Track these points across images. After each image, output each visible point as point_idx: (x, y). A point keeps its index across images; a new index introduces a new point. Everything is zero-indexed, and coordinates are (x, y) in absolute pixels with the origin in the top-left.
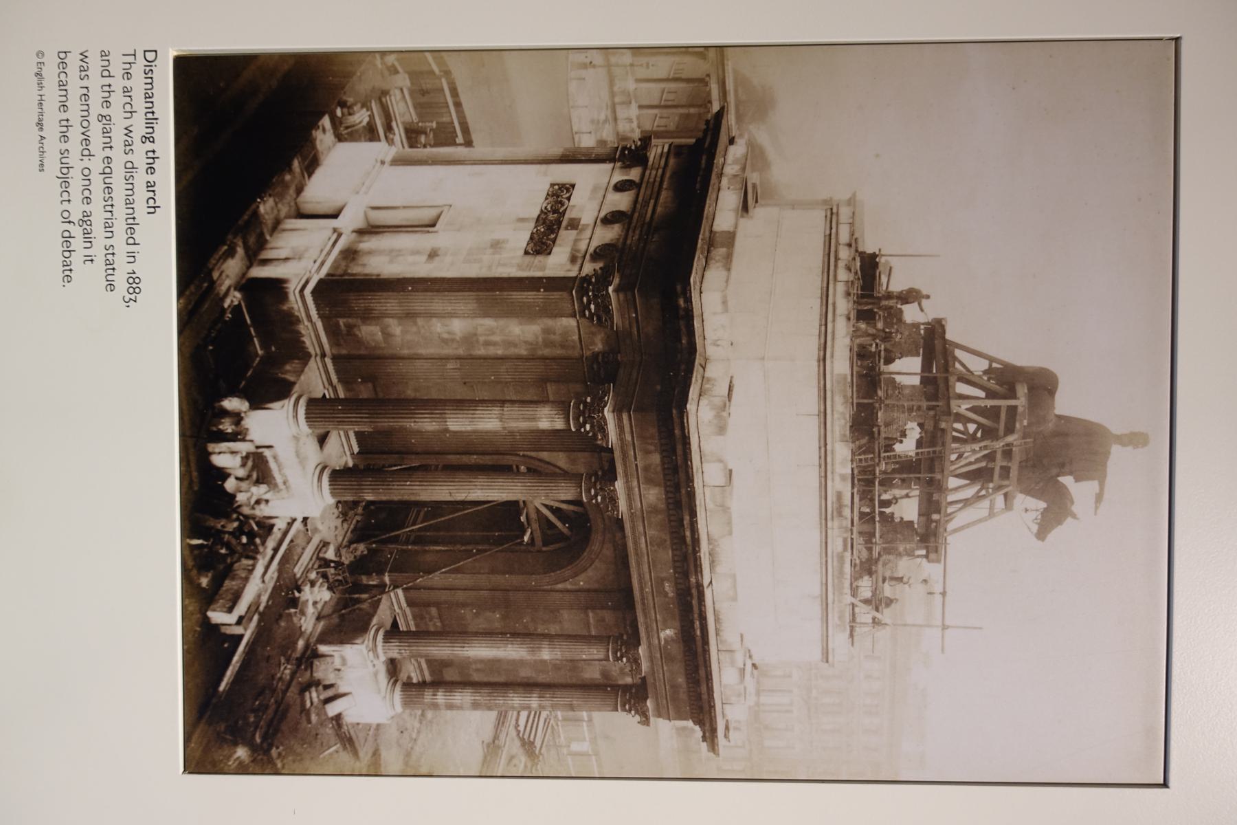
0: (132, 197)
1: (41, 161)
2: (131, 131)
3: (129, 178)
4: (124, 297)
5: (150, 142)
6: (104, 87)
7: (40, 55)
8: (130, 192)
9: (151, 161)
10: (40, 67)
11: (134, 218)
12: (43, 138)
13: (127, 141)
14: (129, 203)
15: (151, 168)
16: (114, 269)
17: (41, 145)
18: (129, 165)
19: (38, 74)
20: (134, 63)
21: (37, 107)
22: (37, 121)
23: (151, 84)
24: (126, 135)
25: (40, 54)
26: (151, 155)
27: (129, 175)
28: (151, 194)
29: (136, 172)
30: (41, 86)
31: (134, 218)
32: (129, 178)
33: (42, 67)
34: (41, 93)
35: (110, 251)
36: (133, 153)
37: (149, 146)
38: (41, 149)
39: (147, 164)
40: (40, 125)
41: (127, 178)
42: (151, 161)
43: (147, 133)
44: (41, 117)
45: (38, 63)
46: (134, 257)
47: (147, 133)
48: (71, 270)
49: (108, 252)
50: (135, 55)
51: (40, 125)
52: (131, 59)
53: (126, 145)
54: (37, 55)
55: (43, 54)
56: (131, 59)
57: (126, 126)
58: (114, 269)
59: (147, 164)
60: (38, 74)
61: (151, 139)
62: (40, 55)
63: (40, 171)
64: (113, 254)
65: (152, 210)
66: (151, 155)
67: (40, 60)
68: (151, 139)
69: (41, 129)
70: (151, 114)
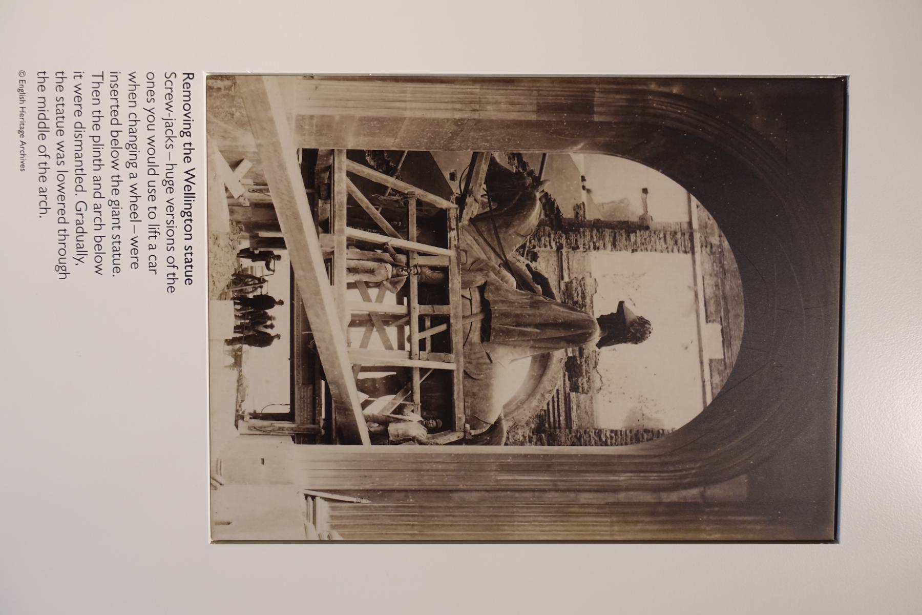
0: (80, 152)
1: (22, 162)
2: (62, 146)
3: (78, 136)
4: (175, 77)
5: (187, 136)
6: (57, 74)
7: (22, 74)
8: (79, 148)
9: (188, 151)
10: (21, 83)
11: (82, 170)
12: (23, 143)
13: (59, 154)
14: (78, 157)
15: (188, 157)
16: (63, 117)
17: (22, 149)
18: (78, 125)
19: (21, 90)
20: (102, 83)
21: (19, 117)
22: (19, 129)
23: (189, 96)
24: (58, 149)
25: (22, 73)
26: (187, 146)
27: (78, 133)
28: (98, 215)
29: (103, 148)
30: (22, 99)
31: (100, 160)
32: (78, 136)
33: (24, 84)
34: (22, 105)
35: (189, 251)
36: (64, 164)
37: (186, 139)
38: (22, 152)
39: (185, 154)
40: (21, 132)
41: (76, 136)
42: (188, 151)
43: (184, 129)
44: (22, 126)
45: (20, 81)
46: (135, 155)
47: (184, 129)
48: (119, 254)
49: (58, 103)
50: (102, 76)
51: (21, 132)
52: (99, 79)
53: (58, 158)
54: (20, 75)
55: (24, 73)
56: (99, 79)
57: (58, 142)
58: (63, 117)
59: (185, 154)
60: (21, 90)
61: (188, 134)
62: (22, 74)
63: (21, 171)
64: (63, 105)
65: (99, 227)
66: (187, 146)
67: (23, 79)
68: (188, 134)
69: (22, 136)
70: (189, 145)
